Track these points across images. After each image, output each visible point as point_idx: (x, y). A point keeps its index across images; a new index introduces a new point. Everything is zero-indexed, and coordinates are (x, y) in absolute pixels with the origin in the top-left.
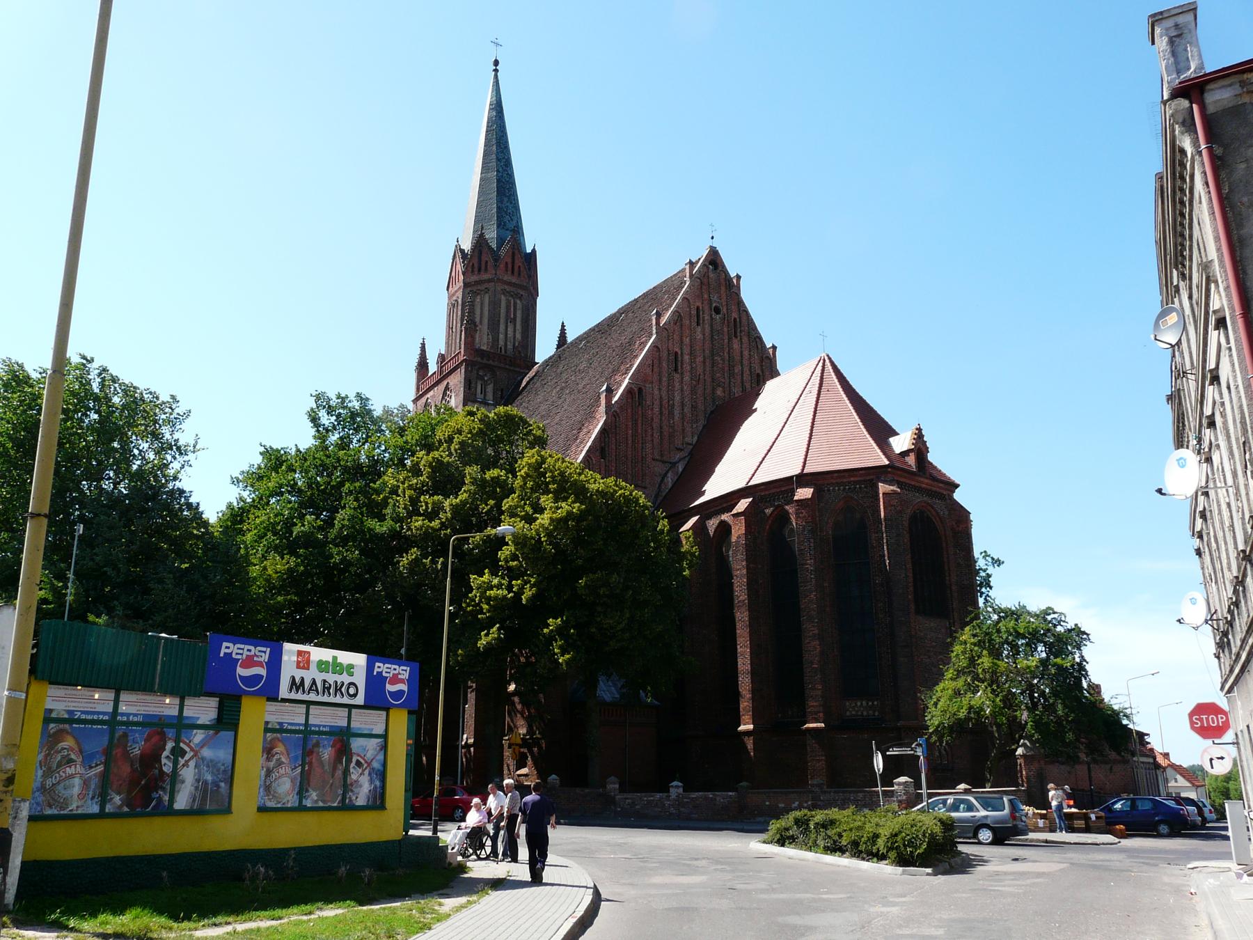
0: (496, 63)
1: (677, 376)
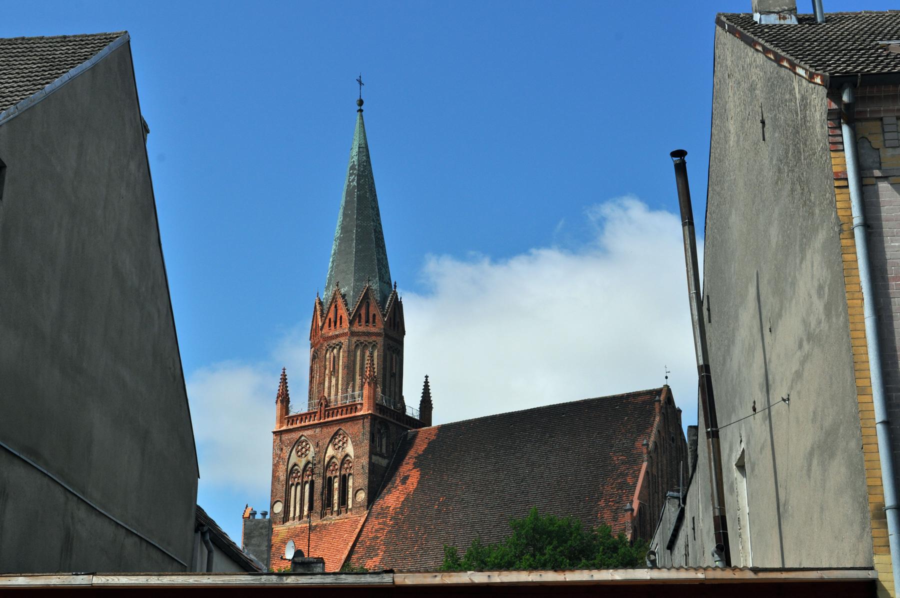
0: (361, 103)
1: (392, 380)
